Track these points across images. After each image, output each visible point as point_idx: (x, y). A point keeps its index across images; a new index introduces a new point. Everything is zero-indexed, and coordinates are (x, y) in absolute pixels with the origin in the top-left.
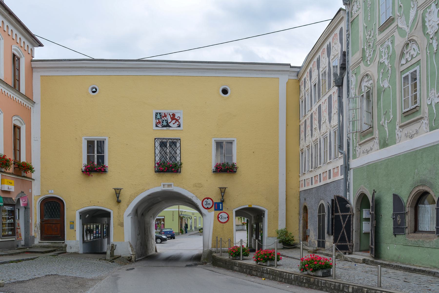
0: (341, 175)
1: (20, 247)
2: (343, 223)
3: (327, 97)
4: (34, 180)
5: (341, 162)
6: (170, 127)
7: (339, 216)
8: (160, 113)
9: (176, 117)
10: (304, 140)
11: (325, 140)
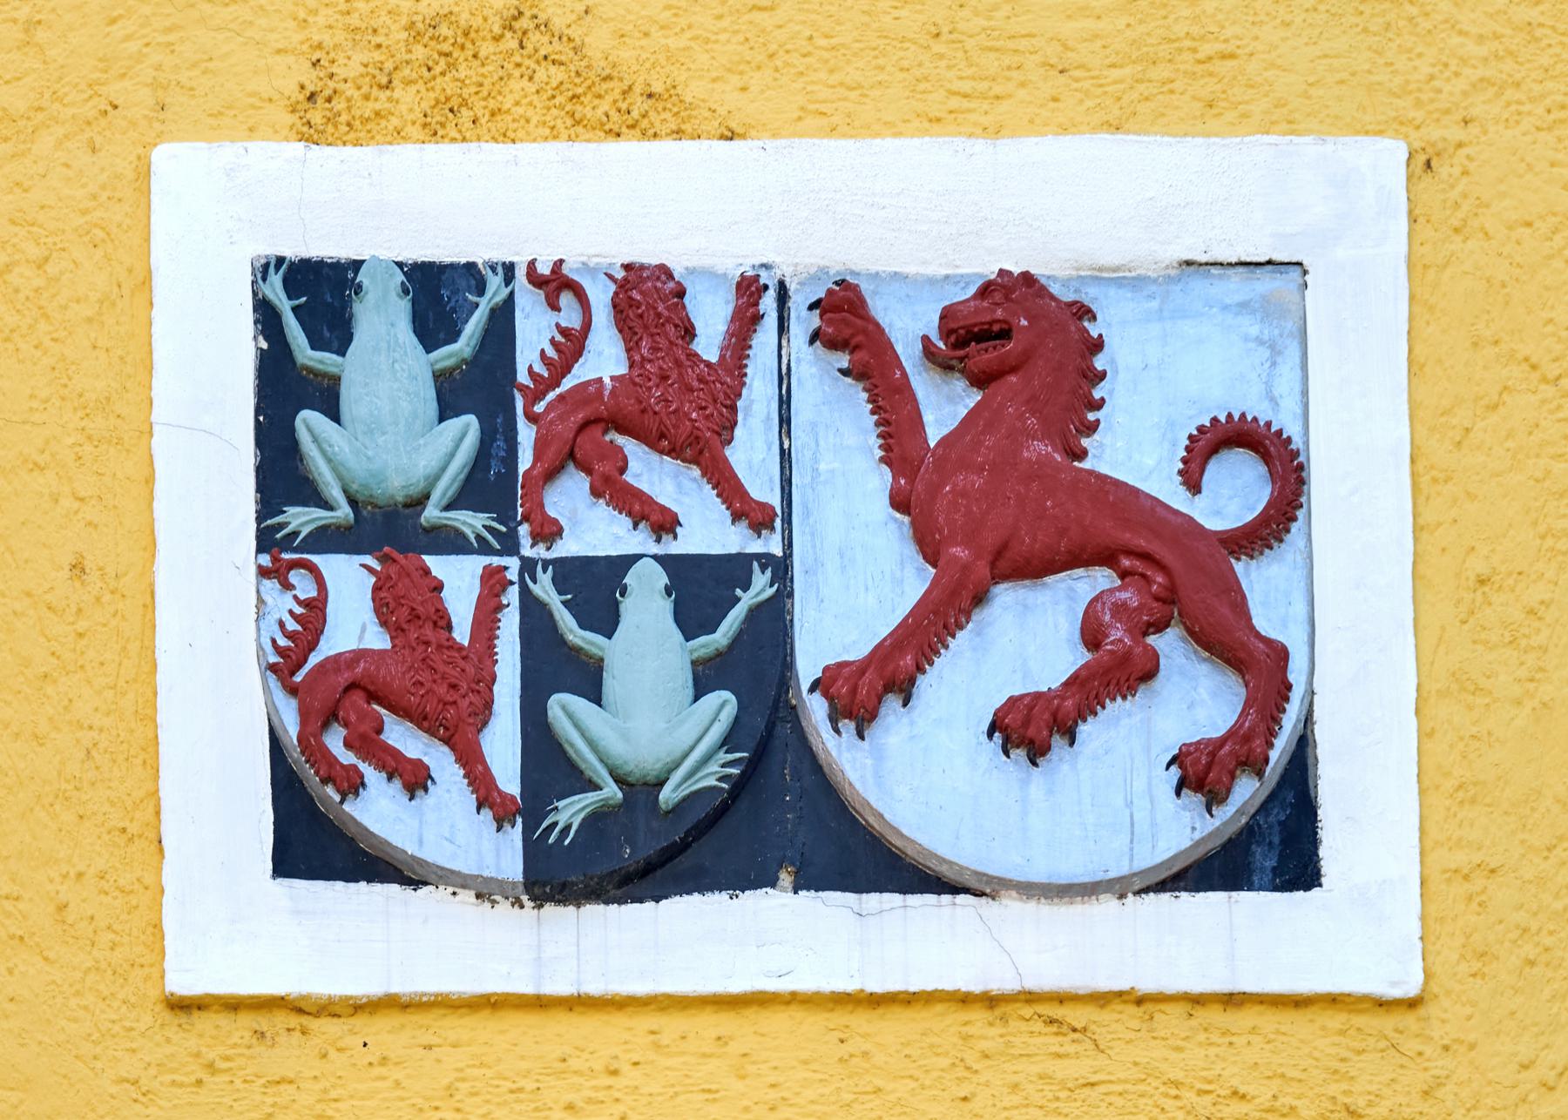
8: (435, 293)
9: (1134, 445)
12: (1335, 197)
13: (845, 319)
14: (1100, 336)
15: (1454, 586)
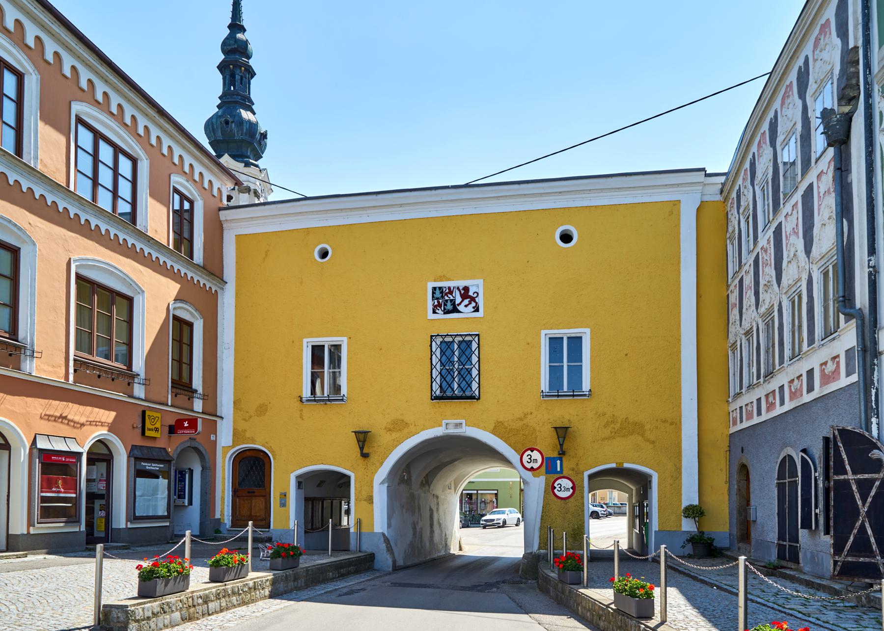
0: (848, 374)
1: (225, 534)
2: (859, 503)
3: (798, 197)
4: (222, 418)
5: (848, 337)
6: (459, 312)
7: (847, 482)
8: (440, 288)
9: (471, 293)
10: (738, 322)
11: (793, 303)
12: (480, 282)
13: (458, 288)
14: (266, 132)
15: (485, 298)
